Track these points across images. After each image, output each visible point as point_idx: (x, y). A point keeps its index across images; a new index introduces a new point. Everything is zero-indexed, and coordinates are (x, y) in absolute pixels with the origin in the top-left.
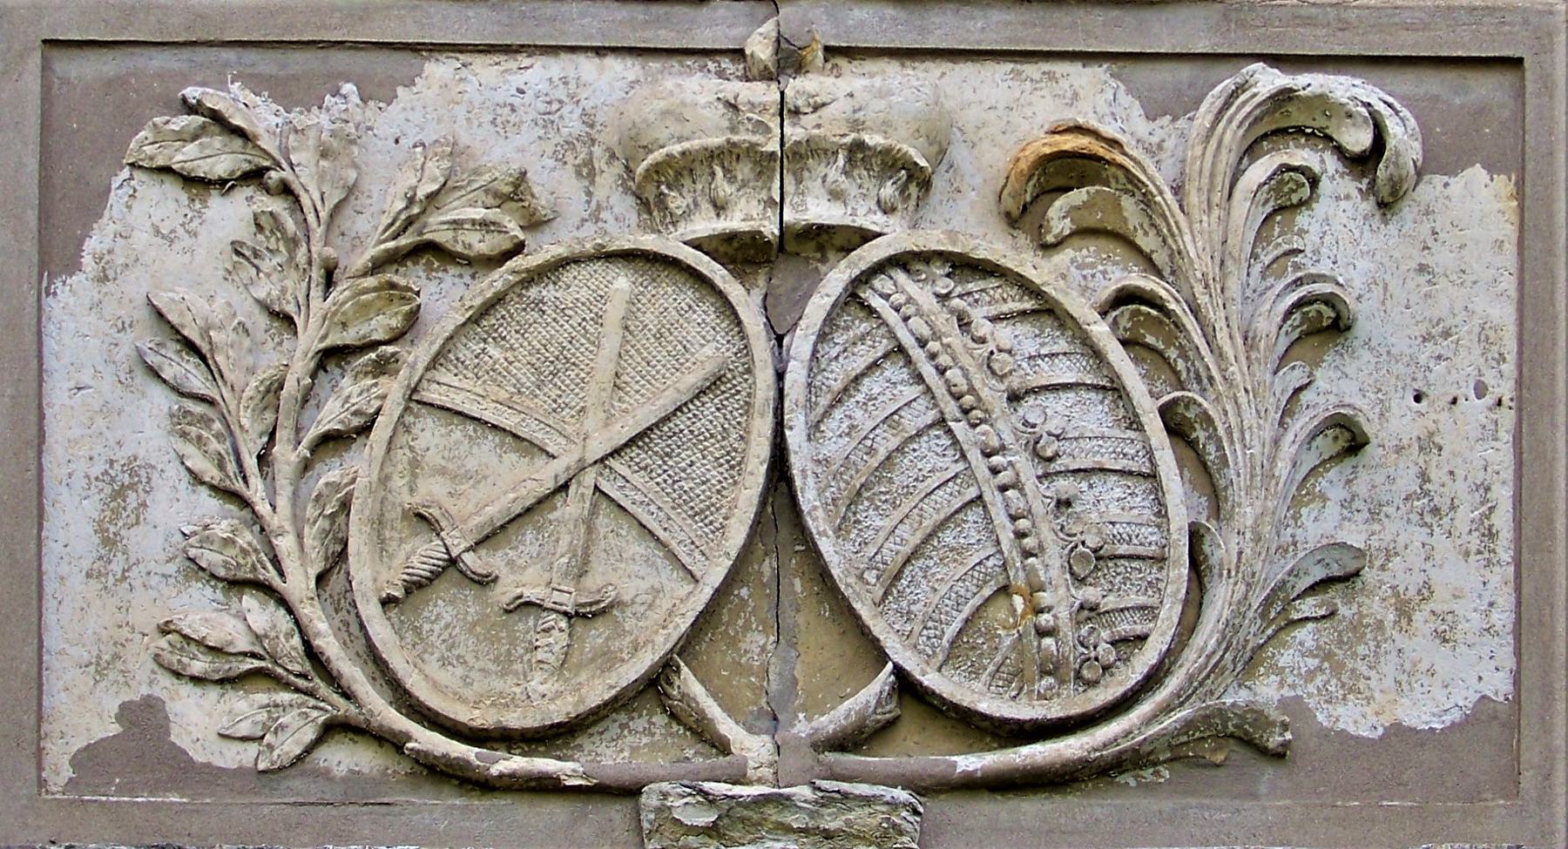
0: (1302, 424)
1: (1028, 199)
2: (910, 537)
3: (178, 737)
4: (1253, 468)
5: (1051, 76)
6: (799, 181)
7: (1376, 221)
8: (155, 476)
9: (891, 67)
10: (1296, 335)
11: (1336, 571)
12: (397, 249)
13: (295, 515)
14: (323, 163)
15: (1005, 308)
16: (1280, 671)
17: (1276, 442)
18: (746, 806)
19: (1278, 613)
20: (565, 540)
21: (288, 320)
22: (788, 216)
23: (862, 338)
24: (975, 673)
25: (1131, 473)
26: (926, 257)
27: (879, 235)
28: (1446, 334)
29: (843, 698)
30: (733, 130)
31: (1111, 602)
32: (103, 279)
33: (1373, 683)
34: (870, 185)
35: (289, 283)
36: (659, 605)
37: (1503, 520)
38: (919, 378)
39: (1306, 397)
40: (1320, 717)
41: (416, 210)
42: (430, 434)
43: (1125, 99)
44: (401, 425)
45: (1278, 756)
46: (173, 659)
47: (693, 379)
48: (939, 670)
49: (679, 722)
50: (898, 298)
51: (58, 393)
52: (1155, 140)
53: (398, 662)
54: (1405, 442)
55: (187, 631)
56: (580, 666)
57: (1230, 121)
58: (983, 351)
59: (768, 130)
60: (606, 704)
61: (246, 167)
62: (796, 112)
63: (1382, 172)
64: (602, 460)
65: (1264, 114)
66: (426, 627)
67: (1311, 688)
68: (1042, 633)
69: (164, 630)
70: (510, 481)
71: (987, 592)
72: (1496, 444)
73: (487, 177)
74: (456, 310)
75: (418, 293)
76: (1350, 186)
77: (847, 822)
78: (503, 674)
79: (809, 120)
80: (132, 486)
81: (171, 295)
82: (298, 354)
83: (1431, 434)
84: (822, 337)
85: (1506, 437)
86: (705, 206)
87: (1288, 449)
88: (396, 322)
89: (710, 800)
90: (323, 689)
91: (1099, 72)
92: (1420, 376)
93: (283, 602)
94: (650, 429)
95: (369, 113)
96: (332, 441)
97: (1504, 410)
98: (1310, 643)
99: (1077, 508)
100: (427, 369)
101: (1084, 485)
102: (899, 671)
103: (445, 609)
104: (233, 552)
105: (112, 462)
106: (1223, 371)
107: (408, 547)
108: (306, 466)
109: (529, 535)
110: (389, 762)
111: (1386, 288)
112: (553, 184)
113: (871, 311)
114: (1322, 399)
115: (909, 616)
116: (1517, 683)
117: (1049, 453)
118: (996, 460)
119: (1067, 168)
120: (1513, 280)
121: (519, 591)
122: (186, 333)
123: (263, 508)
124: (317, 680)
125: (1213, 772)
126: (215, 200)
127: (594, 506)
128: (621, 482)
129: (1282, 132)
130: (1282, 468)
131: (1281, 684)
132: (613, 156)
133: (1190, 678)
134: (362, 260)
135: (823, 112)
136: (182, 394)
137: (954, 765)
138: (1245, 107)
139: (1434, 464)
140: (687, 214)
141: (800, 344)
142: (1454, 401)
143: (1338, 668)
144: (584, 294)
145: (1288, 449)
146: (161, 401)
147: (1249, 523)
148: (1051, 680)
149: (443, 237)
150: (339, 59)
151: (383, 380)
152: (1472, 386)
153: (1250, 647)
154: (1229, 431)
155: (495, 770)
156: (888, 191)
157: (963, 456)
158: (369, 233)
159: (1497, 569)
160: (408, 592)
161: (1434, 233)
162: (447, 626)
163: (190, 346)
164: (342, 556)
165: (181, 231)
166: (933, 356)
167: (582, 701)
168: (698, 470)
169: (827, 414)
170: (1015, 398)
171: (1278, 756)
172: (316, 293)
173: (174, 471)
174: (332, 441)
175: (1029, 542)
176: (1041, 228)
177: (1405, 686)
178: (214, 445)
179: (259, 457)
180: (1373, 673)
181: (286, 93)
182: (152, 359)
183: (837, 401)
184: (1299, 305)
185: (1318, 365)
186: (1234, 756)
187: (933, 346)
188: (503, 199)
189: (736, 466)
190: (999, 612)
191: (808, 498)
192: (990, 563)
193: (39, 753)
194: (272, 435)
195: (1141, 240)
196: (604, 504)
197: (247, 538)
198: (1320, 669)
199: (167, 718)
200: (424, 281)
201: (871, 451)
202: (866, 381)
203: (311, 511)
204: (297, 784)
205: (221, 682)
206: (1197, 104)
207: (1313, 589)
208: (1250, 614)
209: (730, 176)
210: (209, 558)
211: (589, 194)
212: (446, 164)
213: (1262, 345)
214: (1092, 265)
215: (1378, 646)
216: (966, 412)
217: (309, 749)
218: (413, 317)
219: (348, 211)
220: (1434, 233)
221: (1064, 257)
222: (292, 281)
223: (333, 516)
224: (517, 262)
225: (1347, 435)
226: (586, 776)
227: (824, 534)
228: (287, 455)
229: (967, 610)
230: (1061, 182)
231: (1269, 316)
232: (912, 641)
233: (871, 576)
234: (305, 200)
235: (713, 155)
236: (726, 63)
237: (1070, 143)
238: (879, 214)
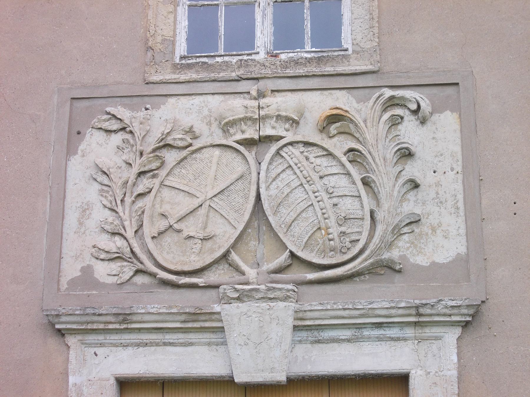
0: (401, 181)
1: (325, 125)
2: (293, 215)
3: (96, 275)
4: (387, 194)
5: (331, 94)
6: (264, 125)
7: (421, 125)
8: (94, 206)
9: (289, 94)
10: (399, 157)
11: (413, 220)
12: (159, 146)
13: (130, 215)
14: (141, 126)
15: (318, 154)
16: (399, 247)
17: (394, 186)
18: (247, 291)
19: (397, 232)
20: (201, 219)
21: (130, 164)
22: (261, 134)
23: (280, 164)
24: (312, 251)
25: (354, 196)
26: (298, 142)
27: (285, 137)
28: (442, 155)
29: (277, 258)
30: (246, 113)
31: (349, 231)
32: (83, 156)
33: (426, 250)
34: (283, 125)
35: (131, 155)
36: (225, 234)
37: (461, 204)
38: (295, 174)
39: (403, 173)
40: (411, 260)
41: (164, 136)
42: (166, 193)
43: (351, 98)
44: (158, 191)
45: (399, 271)
46: (96, 255)
47: (235, 176)
48: (302, 250)
49: (232, 267)
50: (290, 153)
51: (70, 186)
52: (359, 108)
53: (155, 254)
54: (431, 184)
55: (100, 247)
56: (204, 253)
57: (378, 104)
58: (312, 166)
59: (255, 113)
60: (211, 263)
61: (121, 127)
62: (263, 108)
63: (420, 115)
64: (211, 198)
65: (388, 101)
66: (163, 244)
67: (408, 252)
68: (330, 240)
69: (94, 247)
70: (186, 204)
71: (315, 229)
72: (458, 184)
73: (183, 127)
74: (173, 161)
75: (164, 157)
76: (413, 118)
77: (275, 295)
78: (183, 256)
79: (266, 110)
80: (88, 209)
81: (100, 160)
82: (132, 174)
83: (439, 182)
84: (270, 163)
85: (460, 181)
86: (239, 132)
87: (397, 188)
88: (158, 164)
89: (236, 290)
90: (135, 261)
91: (344, 92)
92: (435, 166)
93: (125, 238)
94: (224, 189)
95: (153, 112)
96: (140, 195)
97: (459, 174)
98: (407, 239)
99: (339, 206)
100: (166, 177)
101: (341, 200)
102: (291, 252)
103: (169, 239)
104: (113, 226)
105: (83, 203)
106: (378, 168)
107: (159, 223)
108: (134, 202)
109: (191, 218)
110: (153, 280)
111: (424, 144)
112: (200, 127)
113: (283, 157)
114: (406, 176)
115: (293, 236)
116: (468, 249)
117: (331, 192)
118: (316, 194)
119: (334, 118)
120: (460, 140)
121: (188, 233)
122: (103, 170)
123: (121, 214)
124: (134, 259)
125: (381, 276)
126: (113, 135)
127: (209, 211)
128: (216, 204)
129: (394, 105)
130: (395, 193)
131: (399, 251)
132: (216, 120)
133: (372, 252)
134: (150, 149)
135: (269, 107)
136: (102, 185)
137: (306, 277)
138: (382, 100)
139: (440, 189)
140: (234, 134)
141: (264, 166)
142: (445, 173)
143: (415, 247)
144: (207, 156)
145: (397, 188)
146: (97, 186)
147: (386, 209)
148: (333, 253)
149: (171, 142)
150: (146, 99)
151: (154, 179)
152: (450, 168)
153: (389, 241)
154: (380, 184)
155: (180, 282)
156: (287, 126)
157: (307, 193)
158: (152, 142)
159: (460, 218)
160: (159, 235)
161: (437, 129)
162: (169, 243)
163: (105, 173)
164: (141, 226)
165: (104, 143)
166: (299, 168)
167: (204, 262)
168: (237, 200)
169: (271, 184)
170: (321, 178)
171: (399, 271)
172: (138, 158)
173: (99, 205)
174: (140, 195)
175: (326, 216)
176: (328, 133)
177: (435, 251)
178: (110, 198)
179: (121, 200)
180: (426, 247)
181: (132, 108)
182: (94, 176)
183: (274, 180)
184: (399, 150)
185: (406, 164)
186: (387, 272)
187: (299, 165)
188: (187, 132)
189: (247, 198)
190: (318, 234)
191: (266, 205)
192: (315, 222)
193: (59, 281)
194: (125, 194)
195: (355, 134)
196: (212, 209)
197: (117, 222)
198: (410, 247)
199: (93, 270)
200: (166, 153)
201: (283, 193)
202: (281, 175)
203: (134, 215)
204: (128, 287)
205: (109, 260)
206: (370, 99)
207: (407, 225)
208: (388, 233)
209: (246, 124)
210: (107, 227)
211: (210, 129)
212: (172, 125)
213: (388, 161)
214: (343, 141)
215: (427, 240)
216: (308, 182)
217: (131, 277)
218: (163, 163)
219: (147, 136)
220: (437, 129)
221: (335, 139)
222: (132, 155)
223: (140, 215)
224: (190, 149)
225: (414, 184)
226: (205, 283)
227: (270, 215)
228: (128, 200)
229: (309, 234)
230: (334, 121)
231: (390, 153)
232: (295, 243)
233: (283, 226)
234: (136, 134)
235: (241, 120)
236: (246, 95)
237: (335, 112)
238: (285, 132)
